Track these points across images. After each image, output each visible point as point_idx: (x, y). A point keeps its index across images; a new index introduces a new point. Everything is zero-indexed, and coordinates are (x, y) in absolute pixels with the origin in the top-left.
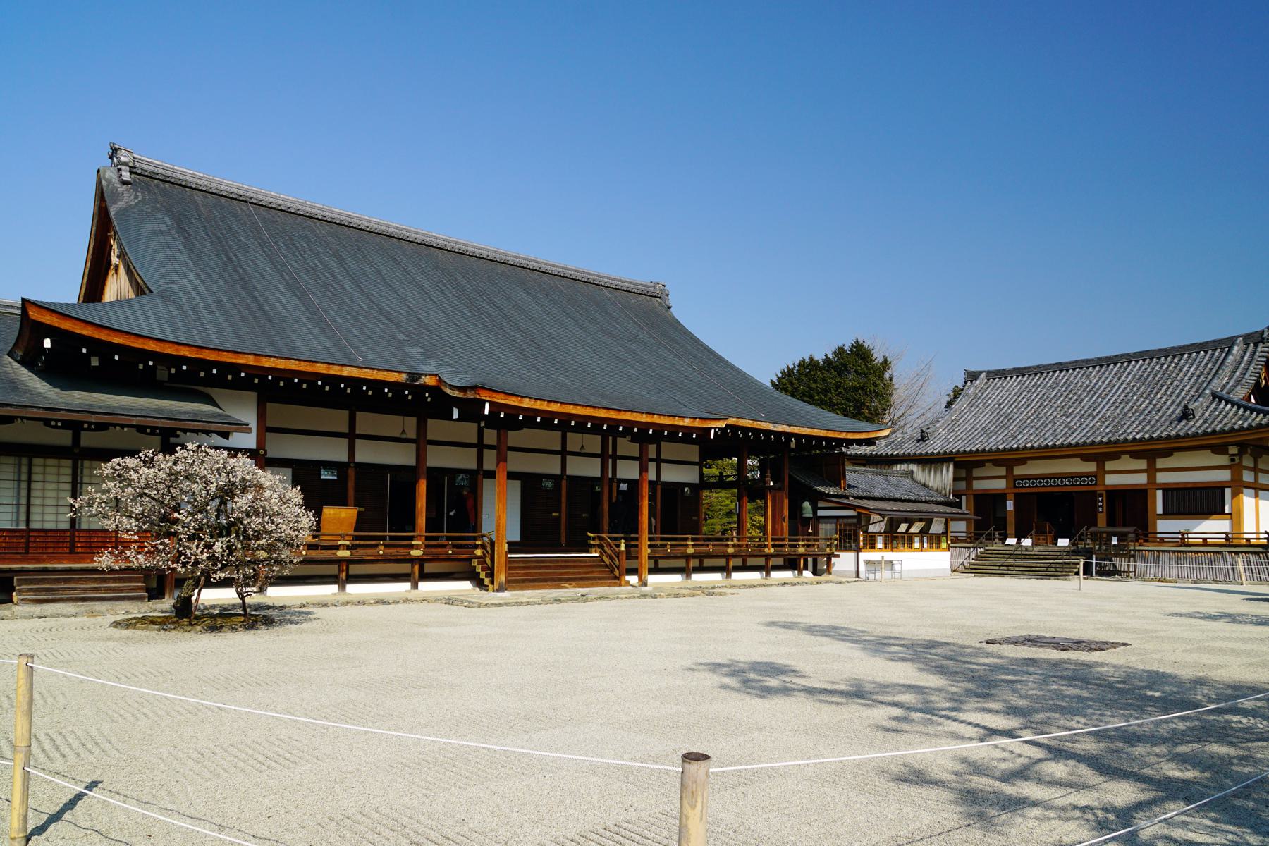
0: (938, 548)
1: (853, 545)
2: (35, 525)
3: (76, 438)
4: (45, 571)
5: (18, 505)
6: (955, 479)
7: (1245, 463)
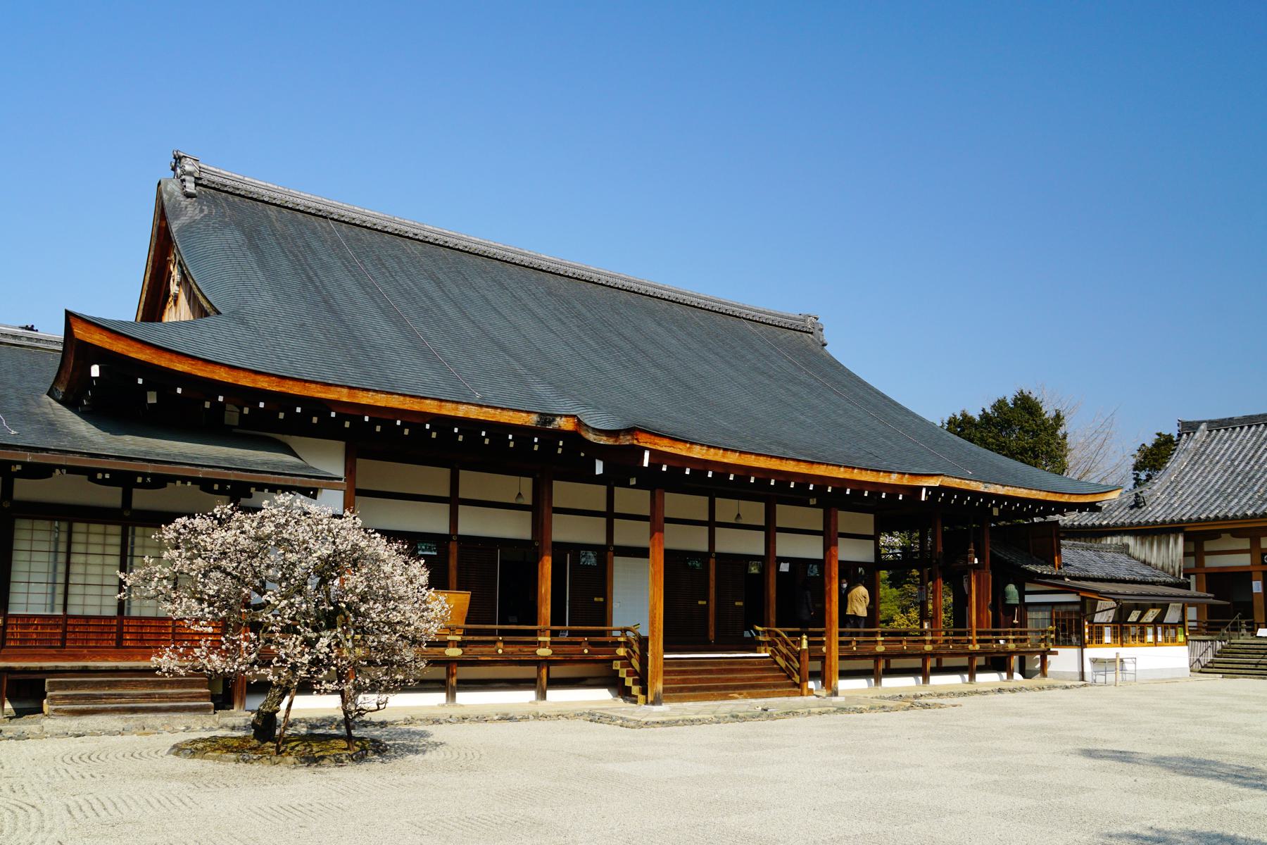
0: (1174, 641)
1: (1074, 638)
2: (74, 611)
3: (127, 498)
4: (85, 671)
5: (54, 583)
6: (1186, 554)
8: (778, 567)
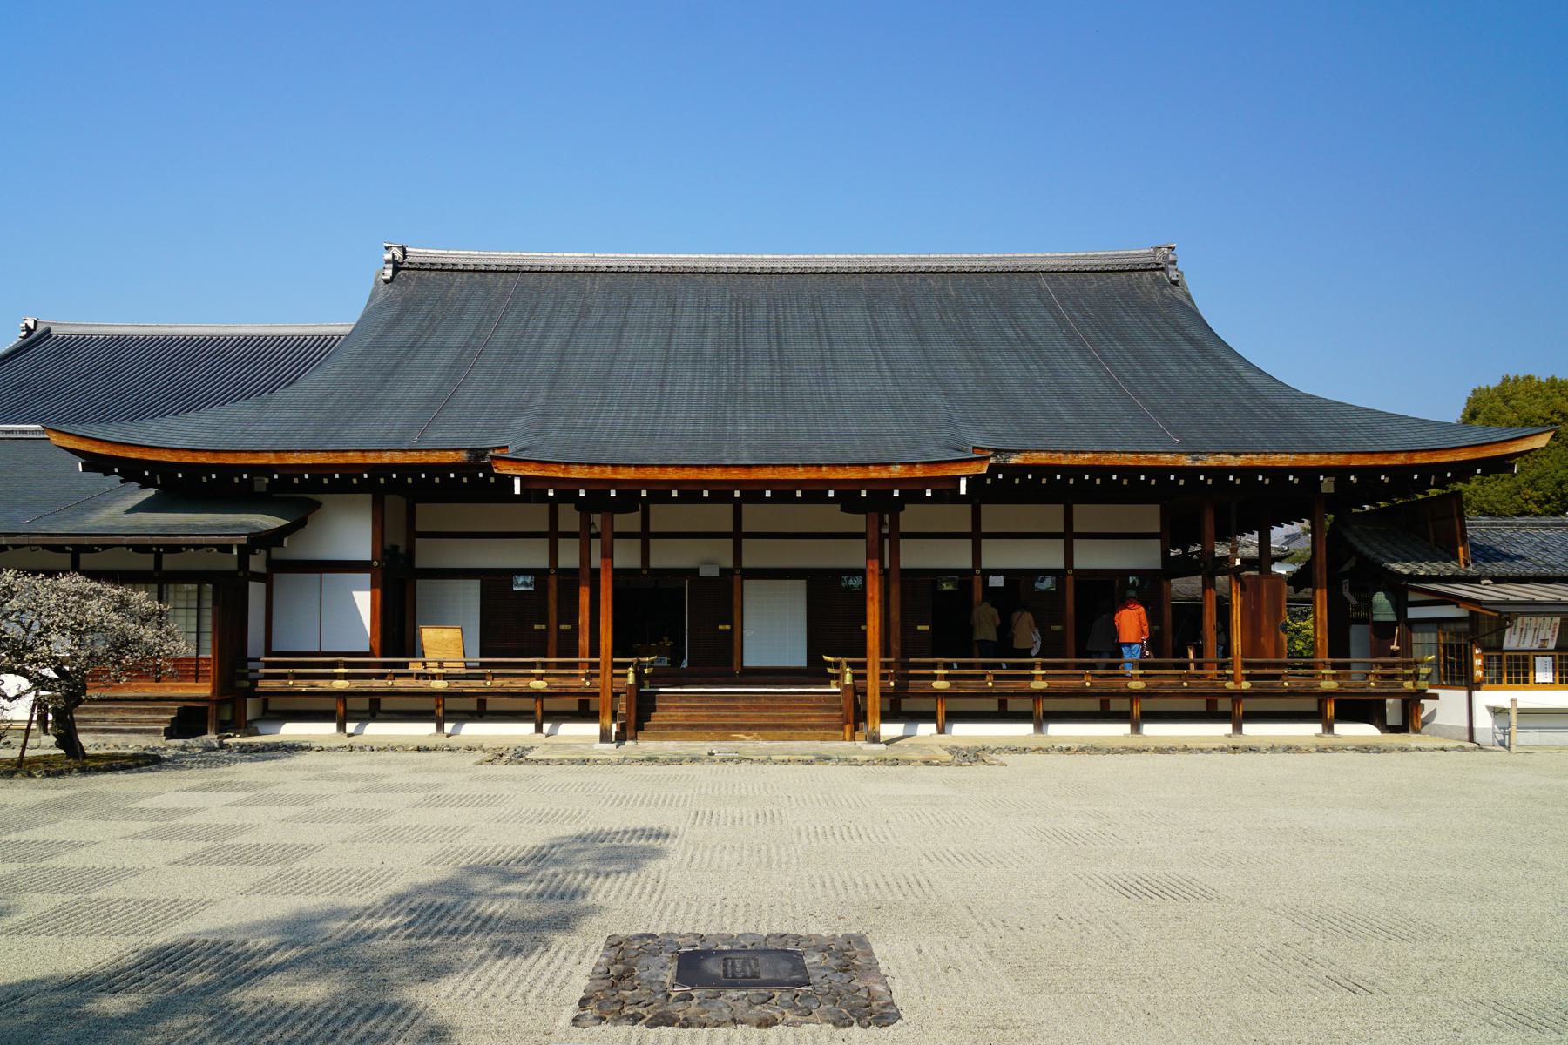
8: (986, 582)
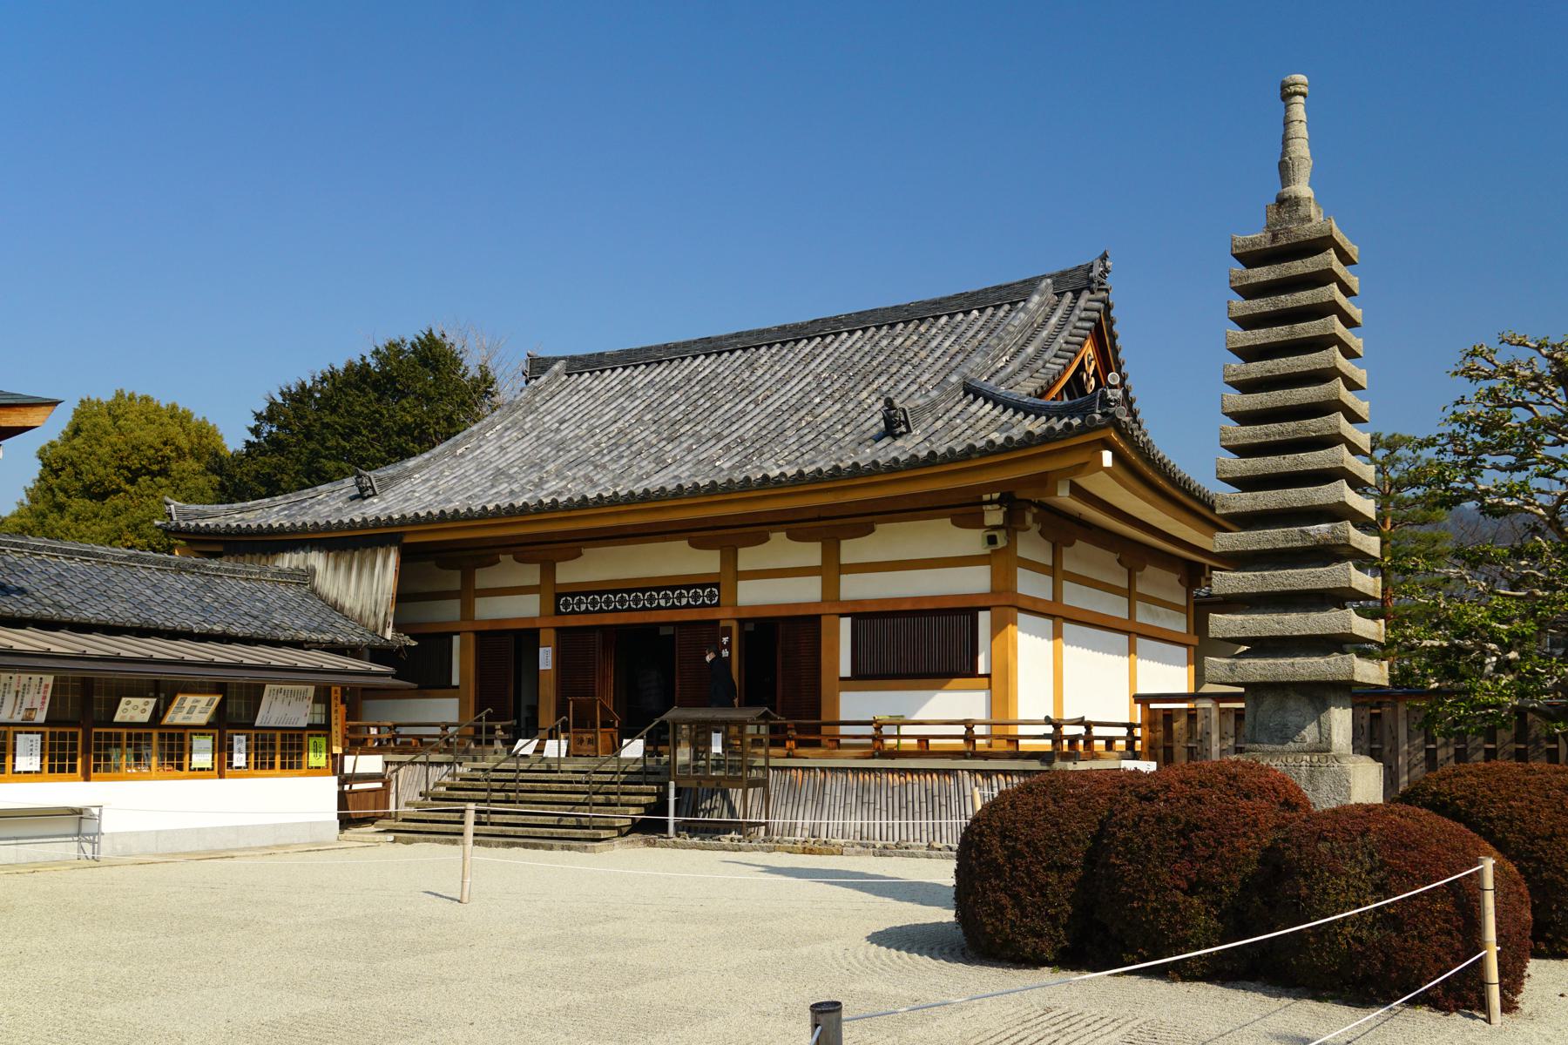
7: (1024, 551)
